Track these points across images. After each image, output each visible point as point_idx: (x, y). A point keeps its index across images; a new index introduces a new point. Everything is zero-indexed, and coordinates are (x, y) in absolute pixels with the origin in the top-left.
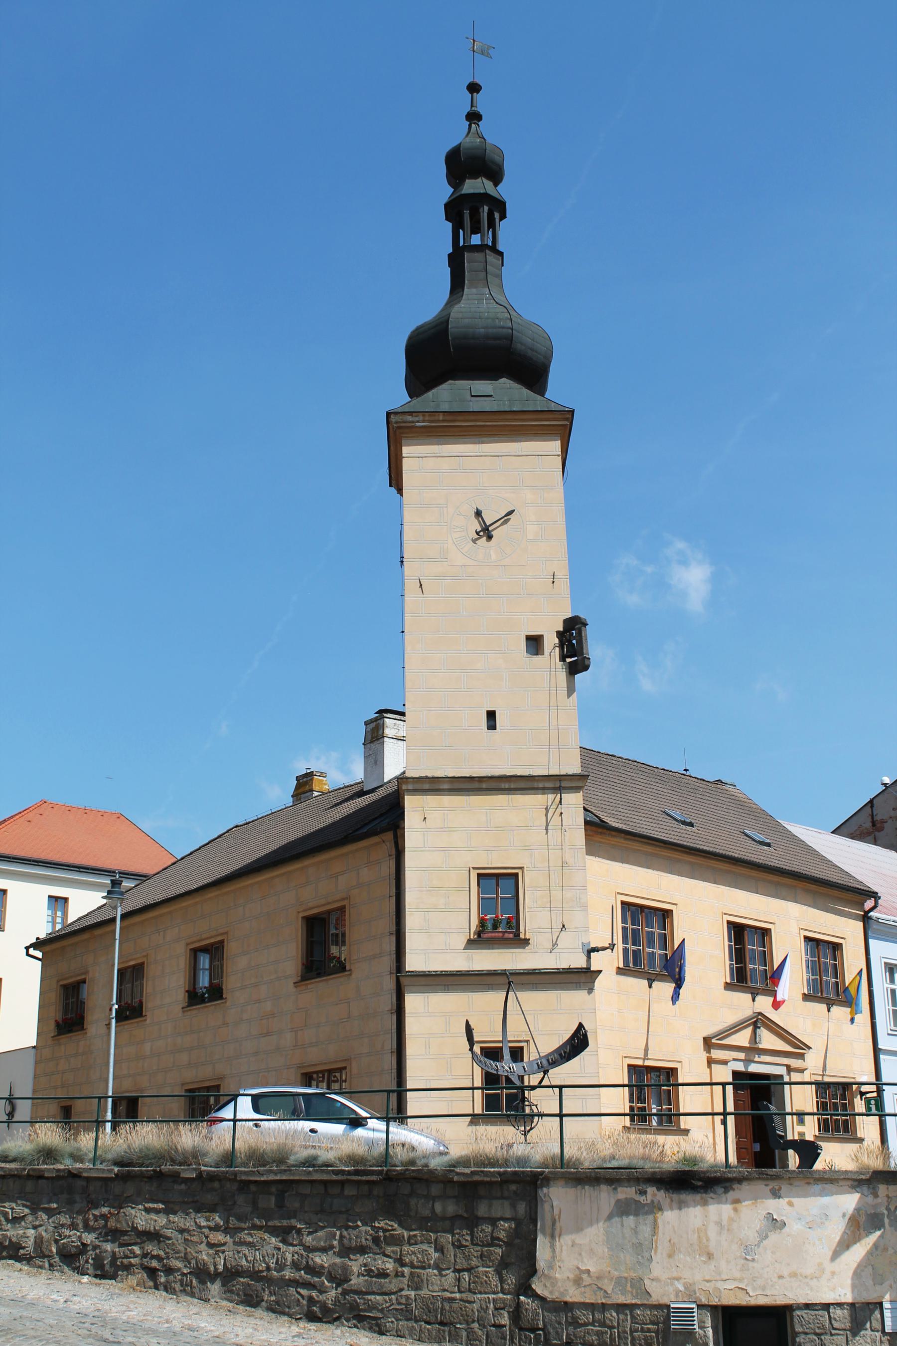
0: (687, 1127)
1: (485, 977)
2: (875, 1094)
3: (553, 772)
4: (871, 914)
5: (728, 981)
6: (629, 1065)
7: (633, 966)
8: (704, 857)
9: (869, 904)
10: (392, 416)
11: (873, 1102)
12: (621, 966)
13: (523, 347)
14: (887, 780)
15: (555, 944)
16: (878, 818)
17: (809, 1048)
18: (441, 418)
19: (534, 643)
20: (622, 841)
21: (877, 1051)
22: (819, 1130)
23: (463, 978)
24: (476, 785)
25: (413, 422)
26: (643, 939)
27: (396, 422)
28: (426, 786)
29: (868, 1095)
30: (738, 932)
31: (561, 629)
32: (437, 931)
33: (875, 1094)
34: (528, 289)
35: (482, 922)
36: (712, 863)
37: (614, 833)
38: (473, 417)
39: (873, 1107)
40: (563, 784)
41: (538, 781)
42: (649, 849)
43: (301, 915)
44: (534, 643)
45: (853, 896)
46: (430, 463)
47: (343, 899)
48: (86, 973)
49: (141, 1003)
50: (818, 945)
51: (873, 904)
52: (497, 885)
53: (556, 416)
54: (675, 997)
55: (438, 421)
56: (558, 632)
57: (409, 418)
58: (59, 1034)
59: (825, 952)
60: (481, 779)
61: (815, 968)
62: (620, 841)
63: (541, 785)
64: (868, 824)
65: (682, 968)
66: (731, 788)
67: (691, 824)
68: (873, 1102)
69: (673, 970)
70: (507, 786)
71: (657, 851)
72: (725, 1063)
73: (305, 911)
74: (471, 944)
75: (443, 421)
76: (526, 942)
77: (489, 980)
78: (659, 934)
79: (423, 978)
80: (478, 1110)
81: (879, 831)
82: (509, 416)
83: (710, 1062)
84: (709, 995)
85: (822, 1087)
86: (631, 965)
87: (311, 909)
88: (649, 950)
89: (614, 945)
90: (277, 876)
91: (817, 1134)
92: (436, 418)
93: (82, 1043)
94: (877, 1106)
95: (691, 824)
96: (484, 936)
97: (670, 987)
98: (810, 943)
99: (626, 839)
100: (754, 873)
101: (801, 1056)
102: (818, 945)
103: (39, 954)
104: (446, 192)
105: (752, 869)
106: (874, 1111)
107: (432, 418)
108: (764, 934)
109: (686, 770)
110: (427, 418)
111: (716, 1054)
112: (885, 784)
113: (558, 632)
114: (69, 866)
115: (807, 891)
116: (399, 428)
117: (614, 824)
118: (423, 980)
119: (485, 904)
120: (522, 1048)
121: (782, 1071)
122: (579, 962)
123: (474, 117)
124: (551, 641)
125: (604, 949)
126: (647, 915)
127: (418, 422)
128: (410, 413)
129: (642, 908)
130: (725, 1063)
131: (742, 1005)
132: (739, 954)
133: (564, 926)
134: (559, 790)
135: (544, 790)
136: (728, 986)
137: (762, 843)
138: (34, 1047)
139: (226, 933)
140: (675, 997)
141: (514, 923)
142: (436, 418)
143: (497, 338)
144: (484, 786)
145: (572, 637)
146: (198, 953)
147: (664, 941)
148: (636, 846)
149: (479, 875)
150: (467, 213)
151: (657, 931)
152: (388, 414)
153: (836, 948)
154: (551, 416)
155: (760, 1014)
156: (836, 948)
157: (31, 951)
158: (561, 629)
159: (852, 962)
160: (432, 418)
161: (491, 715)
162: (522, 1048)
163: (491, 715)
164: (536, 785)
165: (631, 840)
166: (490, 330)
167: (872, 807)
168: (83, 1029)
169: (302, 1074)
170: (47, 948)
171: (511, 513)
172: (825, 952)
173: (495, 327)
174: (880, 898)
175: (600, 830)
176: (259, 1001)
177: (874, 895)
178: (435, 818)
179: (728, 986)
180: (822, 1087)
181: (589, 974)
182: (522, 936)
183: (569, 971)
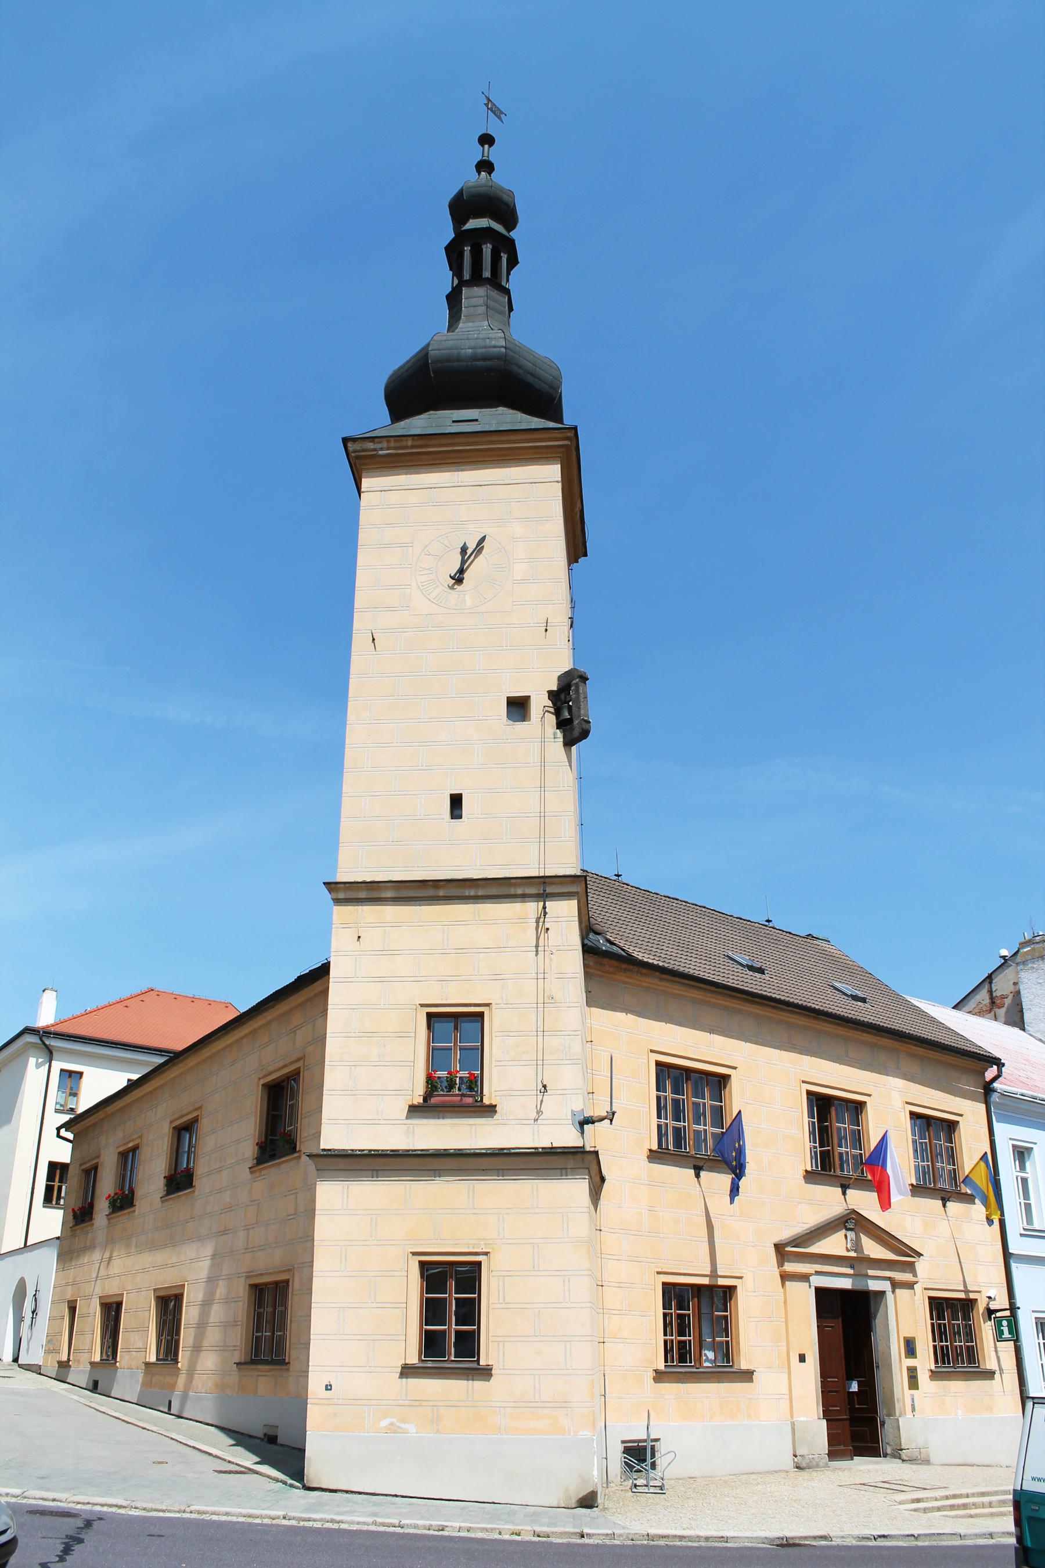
0: (751, 1368)
1: (427, 1160)
2: (1008, 1313)
3: (542, 874)
4: (995, 1085)
5: (809, 1169)
6: (664, 1284)
7: (671, 1149)
8: (773, 1007)
9: (991, 1073)
10: (349, 445)
11: (1005, 1323)
12: (655, 1147)
13: (521, 371)
14: (1004, 952)
15: (539, 1112)
16: (998, 994)
17: (920, 1255)
18: (410, 443)
19: (518, 707)
20: (657, 981)
21: (1007, 1256)
22: (936, 1362)
23: (399, 1159)
24: (431, 892)
25: (375, 450)
26: (689, 1113)
27: (355, 451)
28: (363, 895)
29: (998, 1314)
30: (823, 1107)
31: (555, 689)
32: (365, 1092)
33: (1008, 1313)
34: (539, 319)
35: (430, 1080)
36: (785, 1016)
37: (644, 971)
38: (449, 441)
39: (1006, 1330)
40: (549, 890)
41: (515, 885)
42: (697, 995)
43: (262, 1082)
44: (518, 707)
45: (973, 1067)
46: (394, 497)
47: (298, 1060)
48: (98, 1157)
49: (132, 1191)
50: (929, 1125)
51: (996, 1073)
52: (456, 1028)
53: (555, 435)
54: (735, 1190)
55: (406, 447)
56: (550, 693)
57: (370, 445)
58: (76, 1224)
59: (934, 1130)
60: (436, 883)
61: (923, 1151)
62: (653, 981)
63: (519, 891)
64: (987, 1001)
65: (741, 1152)
66: (824, 944)
67: (761, 971)
68: (1005, 1323)
69: (728, 1157)
70: (472, 893)
71: (707, 997)
72: (805, 1278)
73: (265, 1076)
74: (414, 1110)
75: (412, 447)
76: (490, 1110)
77: (436, 1163)
78: (712, 1106)
79: (340, 1160)
80: (413, 1359)
81: (999, 1008)
82: (494, 438)
83: (785, 1277)
84: (781, 1186)
85: (939, 1306)
86: (671, 1147)
87: (271, 1073)
88: (696, 1127)
89: (614, 1113)
90: (246, 1036)
91: (933, 1368)
92: (404, 444)
93: (90, 1235)
94: (1008, 1323)
95: (761, 971)
96: (434, 1100)
97: (724, 1180)
98: (918, 1122)
99: (661, 979)
100: (842, 1031)
101: (910, 1267)
102: (929, 1125)
103: (70, 1136)
104: (449, 234)
105: (839, 1025)
106: (1006, 1335)
107: (398, 444)
108: (857, 1108)
109: (768, 921)
110: (392, 444)
111: (790, 1267)
112: (1004, 957)
113: (550, 693)
114: (107, 1042)
115: (911, 1055)
116: (357, 457)
117: (640, 957)
118: (341, 1163)
119: (435, 1056)
120: (479, 1264)
121: (886, 1286)
122: (569, 1138)
123: (485, 166)
124: (540, 703)
125: (601, 1119)
126: (696, 1082)
127: (381, 449)
128: (372, 439)
129: (688, 1071)
130: (805, 1278)
131: (830, 1201)
132: (822, 1133)
133: (545, 1086)
134: (544, 897)
135: (524, 897)
136: (810, 1177)
137: (855, 998)
138: (58, 1238)
139: (200, 1108)
140: (735, 1190)
141: (474, 1084)
142: (404, 444)
143: (485, 358)
144: (441, 893)
145: (566, 697)
146: (183, 1132)
147: (718, 1114)
148: (677, 989)
149: (429, 1016)
150: (467, 249)
151: (708, 1102)
152: (345, 441)
153: (950, 1127)
154: (546, 435)
155: (854, 1211)
156: (950, 1127)
157: (63, 1133)
158: (555, 689)
159: (971, 1144)
160: (398, 444)
161: (456, 801)
162: (479, 1264)
163: (456, 801)
164: (512, 891)
165: (668, 980)
166: (479, 351)
167: (991, 983)
168: (91, 1219)
169: (251, 1286)
170: (77, 1128)
171: (483, 539)
172: (934, 1130)
173: (485, 347)
174: (1003, 1065)
175: (624, 966)
176: (220, 1191)
177: (998, 1062)
178: (373, 938)
179: (810, 1177)
180: (939, 1306)
181: (579, 1156)
182: (486, 1101)
183: (551, 1152)
